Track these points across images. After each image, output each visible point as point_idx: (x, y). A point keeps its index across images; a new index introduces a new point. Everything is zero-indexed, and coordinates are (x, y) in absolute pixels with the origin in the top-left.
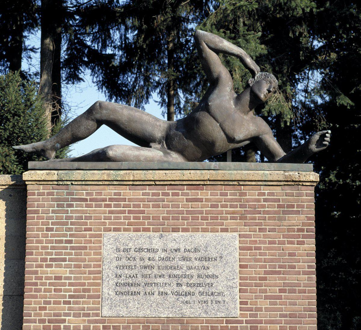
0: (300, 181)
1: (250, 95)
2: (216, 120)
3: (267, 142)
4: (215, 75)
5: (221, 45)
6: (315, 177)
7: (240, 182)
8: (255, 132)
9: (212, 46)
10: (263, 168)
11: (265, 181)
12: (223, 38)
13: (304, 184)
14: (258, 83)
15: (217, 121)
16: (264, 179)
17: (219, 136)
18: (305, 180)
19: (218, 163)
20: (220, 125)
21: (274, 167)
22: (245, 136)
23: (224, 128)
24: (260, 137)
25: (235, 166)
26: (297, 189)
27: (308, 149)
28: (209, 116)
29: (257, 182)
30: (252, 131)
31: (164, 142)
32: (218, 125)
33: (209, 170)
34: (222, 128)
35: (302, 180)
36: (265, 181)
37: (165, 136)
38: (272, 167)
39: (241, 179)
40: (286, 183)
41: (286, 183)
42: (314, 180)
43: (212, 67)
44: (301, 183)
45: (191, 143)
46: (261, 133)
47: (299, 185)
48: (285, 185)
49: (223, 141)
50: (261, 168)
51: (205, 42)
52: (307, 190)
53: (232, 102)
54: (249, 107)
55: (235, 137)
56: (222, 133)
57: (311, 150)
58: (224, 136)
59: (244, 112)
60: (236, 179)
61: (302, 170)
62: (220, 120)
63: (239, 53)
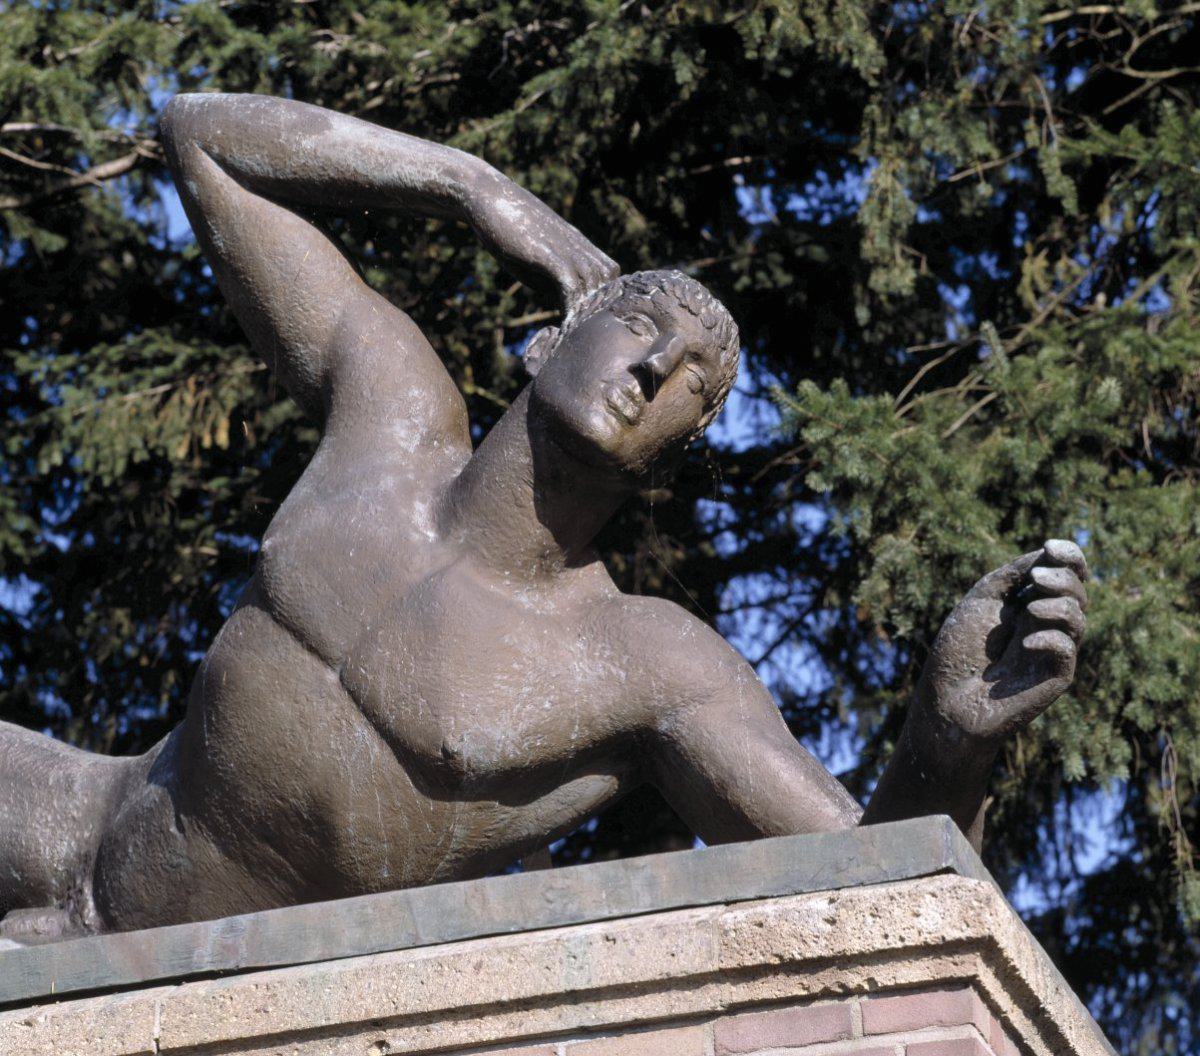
0: (844, 961)
1: (532, 432)
2: (312, 650)
3: (711, 756)
4: (310, 356)
5: (308, 143)
6: (955, 907)
7: (387, 1035)
8: (612, 695)
9: (255, 161)
10: (573, 908)
11: (574, 997)
12: (500, 164)
13: (885, 975)
14: (582, 346)
15: (316, 649)
16: (563, 986)
17: (351, 765)
18: (880, 944)
19: (244, 920)
20: (341, 679)
21: (651, 884)
22: (525, 735)
23: (364, 694)
24: (663, 726)
25: (364, 923)
26: (832, 1027)
27: (937, 719)
28: (271, 627)
29: (515, 1016)
30: (588, 689)
31: (88, 891)
32: (332, 677)
33: (177, 981)
34: (355, 697)
35: (855, 946)
36: (574, 997)
37: (94, 852)
38: (637, 882)
39: (389, 1011)
40: (740, 993)
41: (740, 993)
42: (952, 934)
43: (277, 305)
44: (854, 978)
45: (213, 853)
46: (659, 700)
47: (847, 993)
48: (734, 1009)
49: (384, 788)
50: (557, 906)
51: (207, 150)
52: (913, 1028)
53: (421, 513)
54: (543, 517)
55: (454, 745)
56: (363, 732)
57: (956, 723)
58: (379, 752)
59: (506, 563)
60: (357, 1016)
61: (862, 872)
62: (338, 641)
63: (434, 174)
